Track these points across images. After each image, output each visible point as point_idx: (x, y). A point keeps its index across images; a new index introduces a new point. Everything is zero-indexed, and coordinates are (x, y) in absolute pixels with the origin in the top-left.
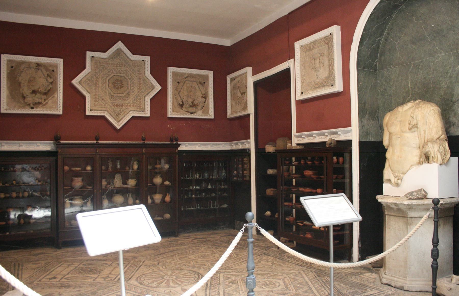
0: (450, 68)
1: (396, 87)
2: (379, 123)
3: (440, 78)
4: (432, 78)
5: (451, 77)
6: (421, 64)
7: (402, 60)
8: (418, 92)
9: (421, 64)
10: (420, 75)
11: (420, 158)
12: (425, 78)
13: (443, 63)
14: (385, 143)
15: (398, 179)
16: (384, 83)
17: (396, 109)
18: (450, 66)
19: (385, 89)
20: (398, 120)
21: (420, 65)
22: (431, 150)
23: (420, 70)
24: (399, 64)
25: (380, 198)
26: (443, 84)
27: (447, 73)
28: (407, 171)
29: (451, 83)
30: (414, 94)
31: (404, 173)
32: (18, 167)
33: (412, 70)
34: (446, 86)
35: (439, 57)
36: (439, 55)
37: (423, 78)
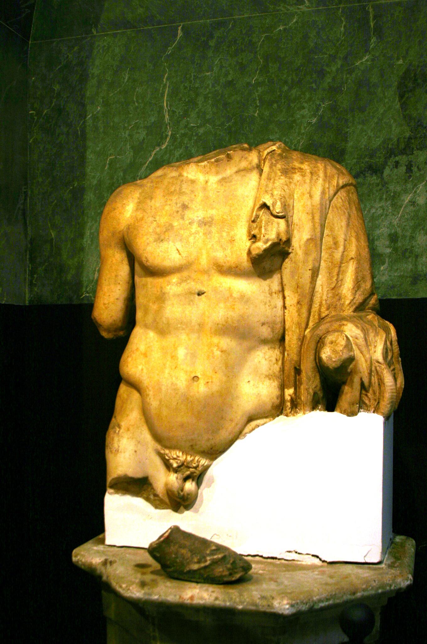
0: (333, 58)
1: (106, 104)
2: (26, 234)
3: (291, 88)
4: (258, 84)
5: (334, 90)
6: (217, 34)
7: (140, 11)
8: (201, 131)
9: (217, 34)
10: (210, 69)
11: (282, 387)
12: (230, 83)
13: (306, 37)
14: (108, 307)
15: (186, 479)
16: (57, 87)
17: (168, 173)
18: (332, 52)
19: (60, 110)
20: (189, 214)
21: (211, 36)
22: (357, 353)
23: (210, 54)
24: (127, 25)
25: (87, 555)
26: (305, 112)
27: (322, 74)
28: (231, 443)
29: (333, 109)
30: (184, 135)
31: (214, 453)
32: (130, 524)
33: (180, 47)
34: (314, 120)
35: (292, 15)
36: (292, 9)
37: (223, 80)
